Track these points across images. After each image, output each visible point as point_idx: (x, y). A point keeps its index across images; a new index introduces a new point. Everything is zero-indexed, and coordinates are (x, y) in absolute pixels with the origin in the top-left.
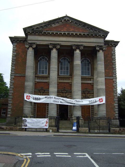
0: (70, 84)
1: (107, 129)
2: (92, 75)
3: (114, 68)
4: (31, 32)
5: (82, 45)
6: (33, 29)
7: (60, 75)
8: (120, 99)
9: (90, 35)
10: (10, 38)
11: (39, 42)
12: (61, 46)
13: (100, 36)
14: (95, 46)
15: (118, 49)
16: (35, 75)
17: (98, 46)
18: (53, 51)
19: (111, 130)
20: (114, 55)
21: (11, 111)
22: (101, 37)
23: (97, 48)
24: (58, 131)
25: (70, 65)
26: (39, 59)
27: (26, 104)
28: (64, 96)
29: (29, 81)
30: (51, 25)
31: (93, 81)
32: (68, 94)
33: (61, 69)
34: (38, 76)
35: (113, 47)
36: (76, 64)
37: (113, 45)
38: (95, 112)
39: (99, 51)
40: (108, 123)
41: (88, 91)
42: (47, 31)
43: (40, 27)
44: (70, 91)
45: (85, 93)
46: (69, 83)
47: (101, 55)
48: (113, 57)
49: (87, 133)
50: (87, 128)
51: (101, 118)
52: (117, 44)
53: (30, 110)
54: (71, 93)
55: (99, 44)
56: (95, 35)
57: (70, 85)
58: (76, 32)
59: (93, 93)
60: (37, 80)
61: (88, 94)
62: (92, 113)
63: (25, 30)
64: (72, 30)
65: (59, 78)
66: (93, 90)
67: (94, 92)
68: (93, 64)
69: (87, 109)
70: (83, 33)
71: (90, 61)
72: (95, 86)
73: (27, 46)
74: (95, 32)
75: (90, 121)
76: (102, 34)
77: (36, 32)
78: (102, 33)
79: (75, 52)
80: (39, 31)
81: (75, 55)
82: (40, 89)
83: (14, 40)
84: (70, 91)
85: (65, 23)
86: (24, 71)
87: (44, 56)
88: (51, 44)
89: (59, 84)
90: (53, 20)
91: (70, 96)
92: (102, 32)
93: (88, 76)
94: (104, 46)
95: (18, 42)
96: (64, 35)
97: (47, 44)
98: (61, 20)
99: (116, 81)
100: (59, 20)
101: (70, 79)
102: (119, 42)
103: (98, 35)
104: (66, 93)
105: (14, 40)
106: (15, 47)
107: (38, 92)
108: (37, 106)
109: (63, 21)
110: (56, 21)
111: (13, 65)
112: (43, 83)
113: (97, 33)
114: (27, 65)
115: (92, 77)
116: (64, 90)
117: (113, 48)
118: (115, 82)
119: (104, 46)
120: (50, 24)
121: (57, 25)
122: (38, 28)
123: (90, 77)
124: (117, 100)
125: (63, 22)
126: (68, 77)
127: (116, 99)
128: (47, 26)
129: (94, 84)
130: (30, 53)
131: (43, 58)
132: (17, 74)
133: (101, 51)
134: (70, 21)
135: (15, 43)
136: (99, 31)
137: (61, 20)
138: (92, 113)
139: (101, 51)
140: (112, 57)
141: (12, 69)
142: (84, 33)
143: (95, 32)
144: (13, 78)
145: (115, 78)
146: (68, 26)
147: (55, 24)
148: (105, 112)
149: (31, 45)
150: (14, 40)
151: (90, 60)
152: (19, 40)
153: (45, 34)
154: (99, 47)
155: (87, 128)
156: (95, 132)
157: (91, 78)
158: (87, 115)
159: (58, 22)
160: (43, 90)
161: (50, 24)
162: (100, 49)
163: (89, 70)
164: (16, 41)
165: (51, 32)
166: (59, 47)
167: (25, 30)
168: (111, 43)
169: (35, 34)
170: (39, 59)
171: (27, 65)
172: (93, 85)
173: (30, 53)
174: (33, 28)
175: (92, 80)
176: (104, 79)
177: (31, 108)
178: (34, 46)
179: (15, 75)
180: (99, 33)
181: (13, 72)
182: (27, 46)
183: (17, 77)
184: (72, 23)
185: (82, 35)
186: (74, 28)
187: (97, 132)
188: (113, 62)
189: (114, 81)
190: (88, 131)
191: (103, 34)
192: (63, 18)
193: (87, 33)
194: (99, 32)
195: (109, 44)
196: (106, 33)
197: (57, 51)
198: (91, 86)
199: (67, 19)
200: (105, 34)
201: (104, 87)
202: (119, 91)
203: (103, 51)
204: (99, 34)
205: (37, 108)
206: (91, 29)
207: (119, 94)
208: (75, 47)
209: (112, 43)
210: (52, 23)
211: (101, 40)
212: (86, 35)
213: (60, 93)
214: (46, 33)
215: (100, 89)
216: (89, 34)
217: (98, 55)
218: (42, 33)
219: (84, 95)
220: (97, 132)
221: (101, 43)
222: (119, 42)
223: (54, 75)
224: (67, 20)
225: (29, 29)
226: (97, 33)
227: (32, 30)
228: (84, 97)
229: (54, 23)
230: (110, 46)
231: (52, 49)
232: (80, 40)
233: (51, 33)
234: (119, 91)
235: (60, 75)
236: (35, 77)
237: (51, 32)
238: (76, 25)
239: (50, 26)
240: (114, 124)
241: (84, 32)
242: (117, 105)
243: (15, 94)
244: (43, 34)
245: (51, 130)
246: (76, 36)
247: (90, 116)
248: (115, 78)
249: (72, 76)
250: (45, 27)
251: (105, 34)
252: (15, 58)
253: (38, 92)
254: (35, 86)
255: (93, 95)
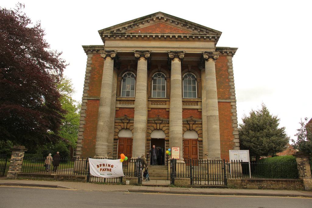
0: (167, 110)
1: (221, 180)
2: (200, 97)
3: (232, 87)
4: (109, 36)
5: (182, 52)
6: (112, 32)
7: (152, 97)
8: (241, 134)
9: (194, 37)
10: (84, 47)
11: (120, 49)
12: (152, 54)
13: (208, 39)
14: (201, 52)
15: (236, 60)
16: (116, 98)
17: (206, 52)
18: (140, 61)
19: (228, 181)
20: (230, 67)
21: (82, 150)
22: (210, 40)
23: (204, 56)
24: (139, 183)
25: (167, 84)
26: (123, 76)
27: (99, 140)
28: (158, 128)
29: (104, 106)
30: (138, 26)
31: (201, 105)
32: (164, 125)
33: (155, 89)
34: (120, 99)
35: (228, 56)
36: (174, 80)
37: (228, 53)
38: (205, 153)
39: (207, 60)
40: (223, 170)
41: (193, 121)
42: (131, 33)
43: (123, 28)
44: (166, 121)
45: (189, 124)
46: (165, 109)
47: (211, 65)
48: (229, 70)
49: (189, 187)
50: (188, 177)
51: (213, 162)
52: (235, 52)
53: (105, 149)
54: (169, 123)
55: (208, 51)
56: (201, 37)
57: (167, 112)
58: (173, 34)
59: (201, 124)
60: (119, 106)
61: (193, 125)
62: (201, 154)
63: (101, 33)
64: (167, 31)
65: (150, 102)
66: (201, 118)
67: (202, 122)
68: (201, 81)
69: (193, 147)
70: (184, 35)
71: (196, 77)
72: (204, 114)
73: (104, 56)
74: (201, 33)
75: (192, 167)
76: (211, 36)
77: (116, 36)
78: (212, 34)
79: (172, 62)
80: (120, 34)
81: (172, 67)
82: (123, 118)
83: (89, 50)
84: (166, 121)
85: (157, 22)
86: (99, 92)
87: (130, 71)
88: (137, 51)
89: (150, 112)
90: (140, 18)
91: (167, 128)
92: (211, 33)
93: (193, 99)
94: (215, 53)
95: (95, 52)
96: (157, 38)
97: (131, 51)
98: (151, 18)
99: (235, 105)
100: (149, 19)
101: (167, 102)
102: (238, 48)
103: (205, 38)
104: (160, 124)
105: (88, 49)
106: (90, 59)
107: (120, 122)
108: (119, 143)
109: (154, 19)
110: (145, 20)
111: (86, 85)
112: (126, 110)
113: (203, 34)
114: (102, 82)
115: (200, 100)
116: (159, 120)
117: (229, 57)
118: (234, 107)
119: (215, 53)
120: (136, 24)
121: (146, 25)
122: (119, 29)
123: (196, 100)
124: (237, 133)
125: (154, 21)
126: (164, 100)
127: (236, 139)
128: (132, 28)
129: (203, 110)
130: (109, 64)
131: (129, 74)
132: (91, 97)
133: (211, 60)
134: (165, 19)
135: (90, 54)
136: (207, 31)
137: (151, 18)
138: (201, 154)
139: (211, 60)
140: (227, 70)
141: (85, 90)
142: (185, 35)
143: (201, 33)
144: (86, 103)
145: (233, 101)
146: (161, 26)
147: (143, 24)
148: (220, 152)
149: (109, 53)
150: (88, 49)
151: (196, 76)
152: (95, 50)
153: (129, 38)
154: (207, 55)
155: (188, 178)
156: (201, 184)
157: (198, 102)
158: (194, 156)
159: (147, 21)
160: (128, 120)
161: (136, 24)
162: (209, 57)
163: (194, 89)
164: (92, 51)
165: (138, 34)
166: (149, 55)
167: (101, 33)
168: (225, 51)
169: (115, 38)
170: (123, 76)
171: (102, 82)
172: (201, 112)
173: (108, 64)
174: (112, 30)
175: (199, 103)
176: (217, 101)
177: (108, 146)
178: (114, 55)
179: (88, 99)
180: (206, 35)
181: (86, 95)
182: (104, 56)
183: (91, 101)
184: (168, 22)
185: (182, 37)
186: (171, 28)
187: (205, 184)
188: (230, 77)
189: (232, 105)
190: (190, 183)
191: (213, 36)
192: (154, 15)
193: (190, 35)
194: (206, 32)
195: (223, 52)
196: (216, 35)
197: (147, 61)
198: (198, 113)
199: (160, 16)
200: (216, 36)
201: (217, 113)
202: (240, 122)
203: (214, 59)
204: (207, 35)
205: (119, 147)
206: (196, 29)
207: (240, 125)
208: (172, 54)
209: (227, 51)
210: (139, 22)
211: (211, 45)
212: (188, 37)
213: (153, 123)
214: (130, 36)
215: (211, 116)
216: (192, 35)
217: (206, 66)
218: (124, 36)
219: (188, 126)
220: (205, 184)
221: (210, 48)
222: (238, 48)
223: (141, 95)
224: (160, 18)
225: (107, 32)
226: (203, 34)
227: (111, 33)
228: (187, 130)
229: (142, 23)
230: (225, 56)
231: (138, 59)
232: (180, 45)
233: (137, 36)
234: (240, 122)
235: (152, 97)
236: (116, 100)
237: (138, 34)
238: (173, 24)
239: (136, 27)
240: (40, 168)
241: (185, 34)
242: (238, 141)
243: (89, 125)
244: (126, 38)
245: (129, 181)
246: (174, 39)
247: (197, 158)
248: (233, 101)
249: (169, 99)
250: (130, 29)
251: (216, 36)
252: (89, 75)
253: (120, 122)
254: (116, 114)
255: (202, 127)
